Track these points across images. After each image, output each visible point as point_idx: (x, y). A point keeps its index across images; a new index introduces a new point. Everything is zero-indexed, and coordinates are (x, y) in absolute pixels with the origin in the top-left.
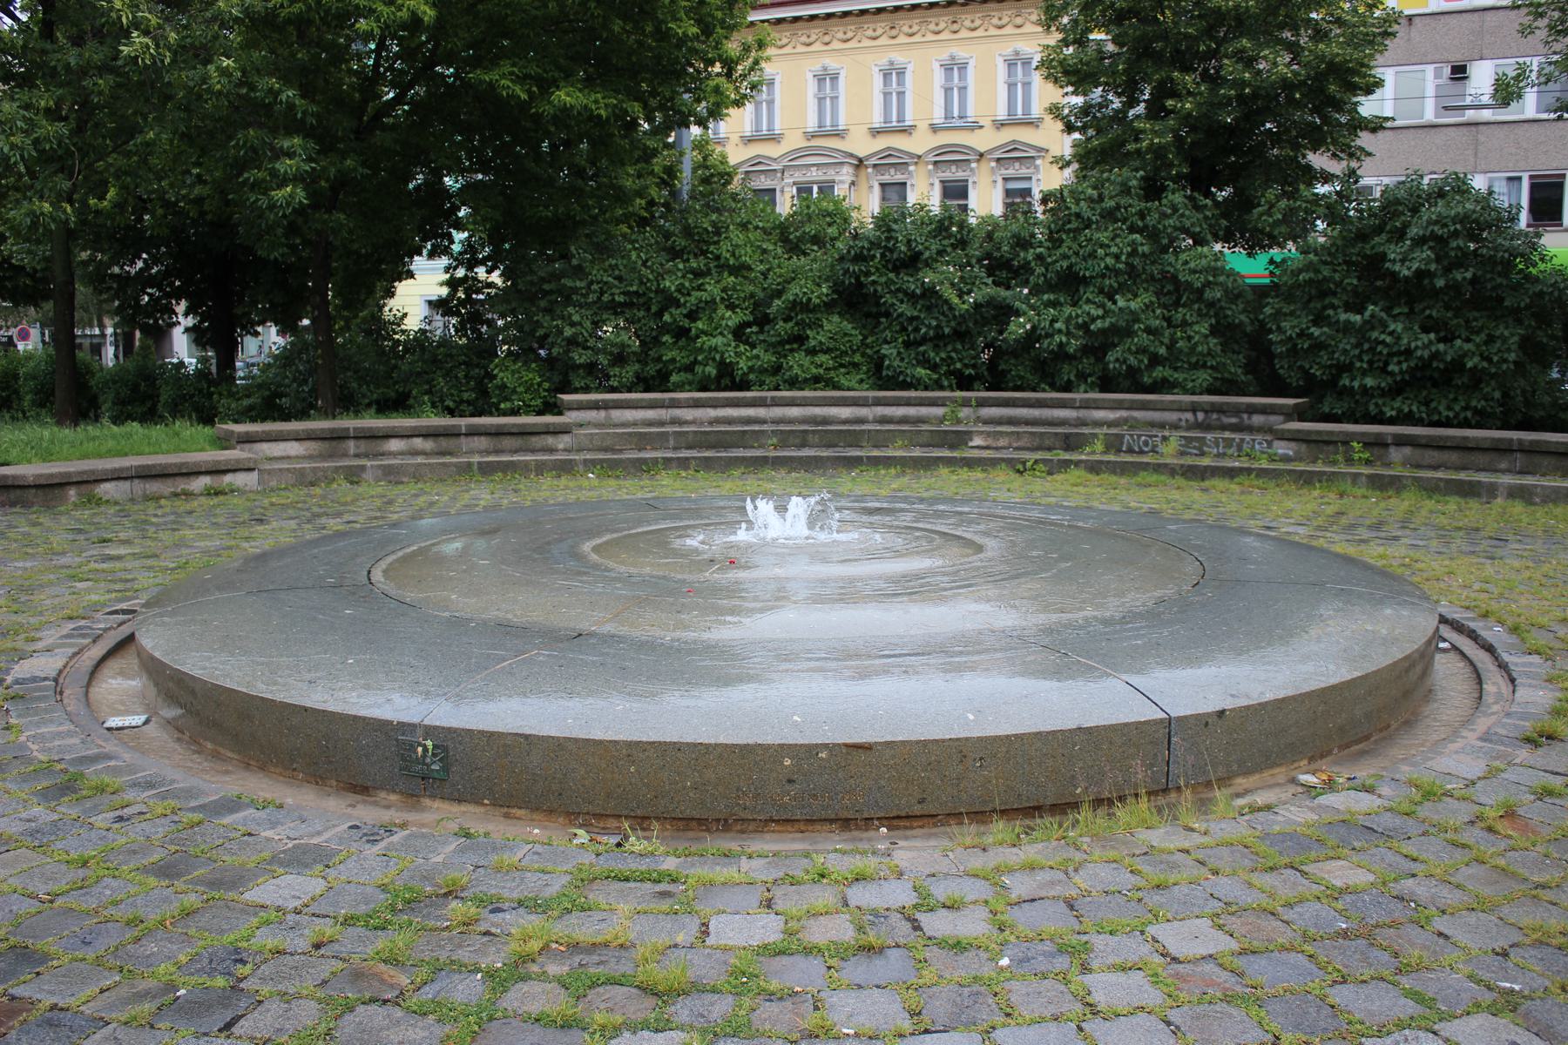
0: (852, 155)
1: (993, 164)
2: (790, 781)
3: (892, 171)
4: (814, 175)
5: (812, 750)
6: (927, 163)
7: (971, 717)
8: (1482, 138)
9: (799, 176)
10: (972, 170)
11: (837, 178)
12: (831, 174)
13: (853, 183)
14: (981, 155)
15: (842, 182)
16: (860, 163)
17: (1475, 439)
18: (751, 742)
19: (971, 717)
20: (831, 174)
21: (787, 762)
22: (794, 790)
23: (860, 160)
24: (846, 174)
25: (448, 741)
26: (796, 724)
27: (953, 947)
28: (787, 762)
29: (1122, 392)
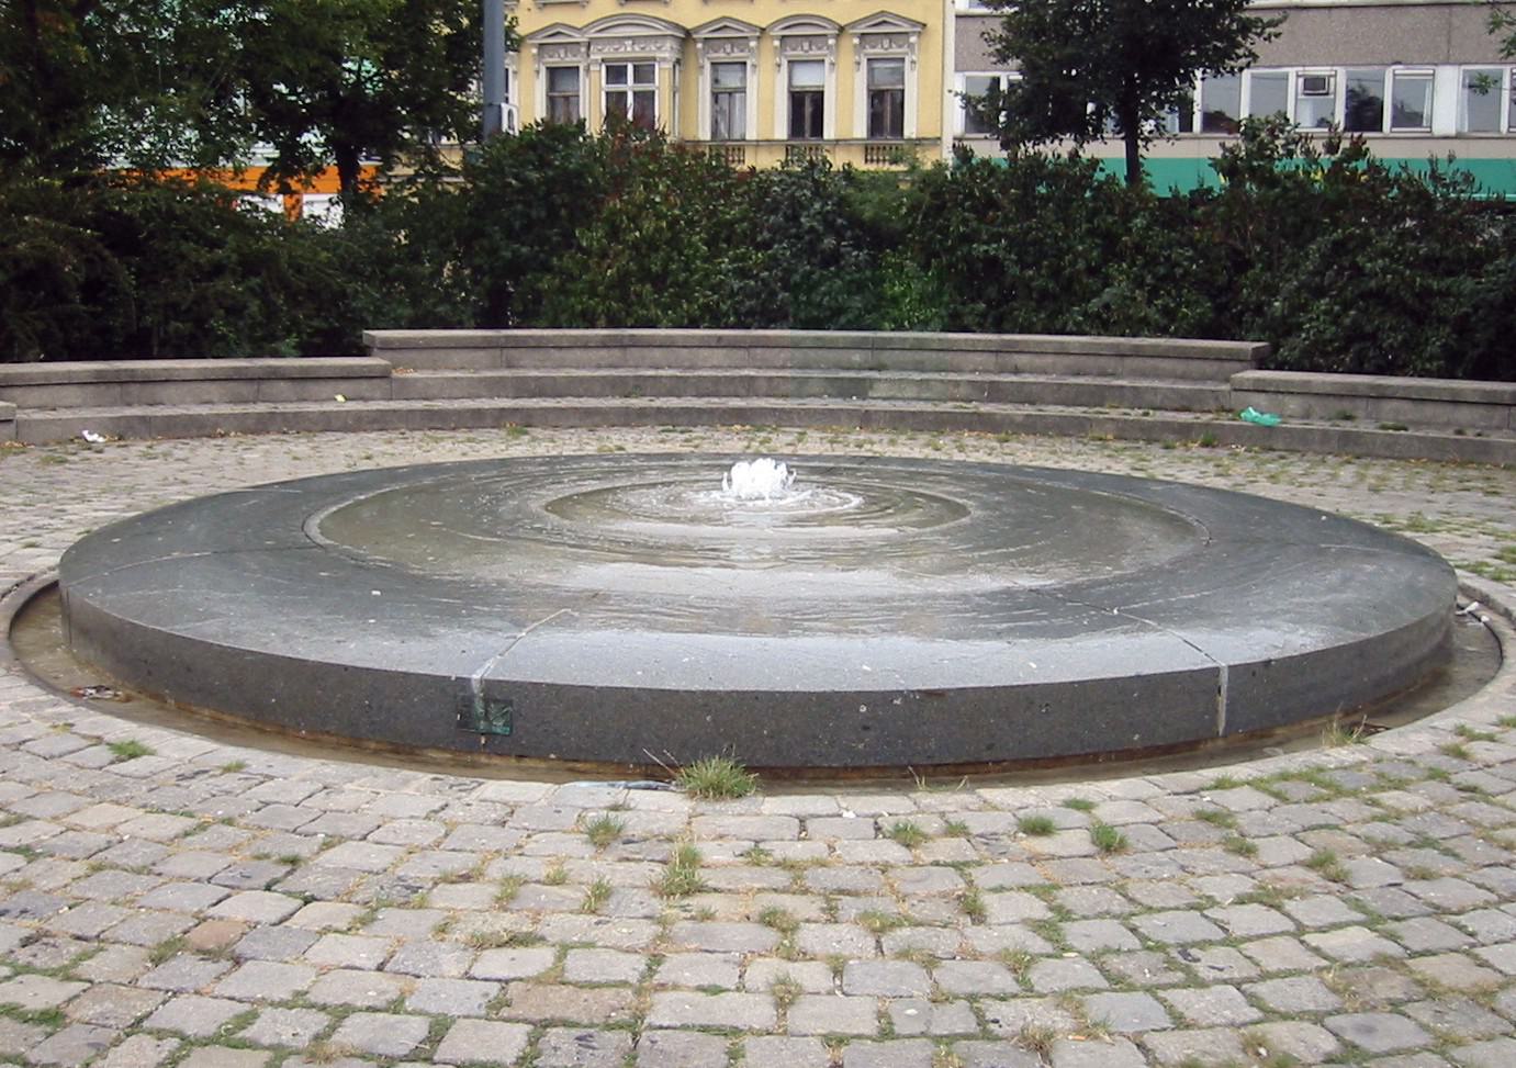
0: (677, 26)
1: (856, 41)
2: (866, 728)
3: (886, 43)
4: (628, 50)
5: (886, 697)
6: (773, 38)
7: (1034, 666)
8: (1456, 22)
9: (609, 52)
10: (911, 46)
11: (659, 55)
12: (651, 50)
13: (678, 61)
14: (842, 29)
15: (664, 60)
16: (686, 37)
17: (143, 371)
18: (828, 689)
19: (1034, 666)
20: (651, 50)
21: (863, 709)
22: (869, 737)
23: (688, 33)
24: (667, 52)
25: (500, 694)
26: (866, 672)
27: (1029, 860)
28: (863, 709)
29: (1037, 333)
